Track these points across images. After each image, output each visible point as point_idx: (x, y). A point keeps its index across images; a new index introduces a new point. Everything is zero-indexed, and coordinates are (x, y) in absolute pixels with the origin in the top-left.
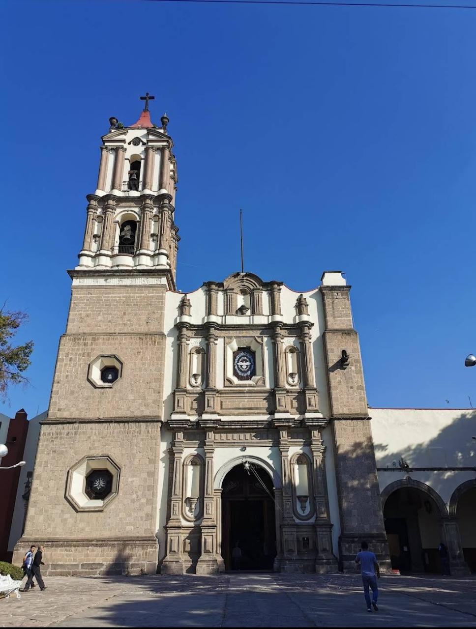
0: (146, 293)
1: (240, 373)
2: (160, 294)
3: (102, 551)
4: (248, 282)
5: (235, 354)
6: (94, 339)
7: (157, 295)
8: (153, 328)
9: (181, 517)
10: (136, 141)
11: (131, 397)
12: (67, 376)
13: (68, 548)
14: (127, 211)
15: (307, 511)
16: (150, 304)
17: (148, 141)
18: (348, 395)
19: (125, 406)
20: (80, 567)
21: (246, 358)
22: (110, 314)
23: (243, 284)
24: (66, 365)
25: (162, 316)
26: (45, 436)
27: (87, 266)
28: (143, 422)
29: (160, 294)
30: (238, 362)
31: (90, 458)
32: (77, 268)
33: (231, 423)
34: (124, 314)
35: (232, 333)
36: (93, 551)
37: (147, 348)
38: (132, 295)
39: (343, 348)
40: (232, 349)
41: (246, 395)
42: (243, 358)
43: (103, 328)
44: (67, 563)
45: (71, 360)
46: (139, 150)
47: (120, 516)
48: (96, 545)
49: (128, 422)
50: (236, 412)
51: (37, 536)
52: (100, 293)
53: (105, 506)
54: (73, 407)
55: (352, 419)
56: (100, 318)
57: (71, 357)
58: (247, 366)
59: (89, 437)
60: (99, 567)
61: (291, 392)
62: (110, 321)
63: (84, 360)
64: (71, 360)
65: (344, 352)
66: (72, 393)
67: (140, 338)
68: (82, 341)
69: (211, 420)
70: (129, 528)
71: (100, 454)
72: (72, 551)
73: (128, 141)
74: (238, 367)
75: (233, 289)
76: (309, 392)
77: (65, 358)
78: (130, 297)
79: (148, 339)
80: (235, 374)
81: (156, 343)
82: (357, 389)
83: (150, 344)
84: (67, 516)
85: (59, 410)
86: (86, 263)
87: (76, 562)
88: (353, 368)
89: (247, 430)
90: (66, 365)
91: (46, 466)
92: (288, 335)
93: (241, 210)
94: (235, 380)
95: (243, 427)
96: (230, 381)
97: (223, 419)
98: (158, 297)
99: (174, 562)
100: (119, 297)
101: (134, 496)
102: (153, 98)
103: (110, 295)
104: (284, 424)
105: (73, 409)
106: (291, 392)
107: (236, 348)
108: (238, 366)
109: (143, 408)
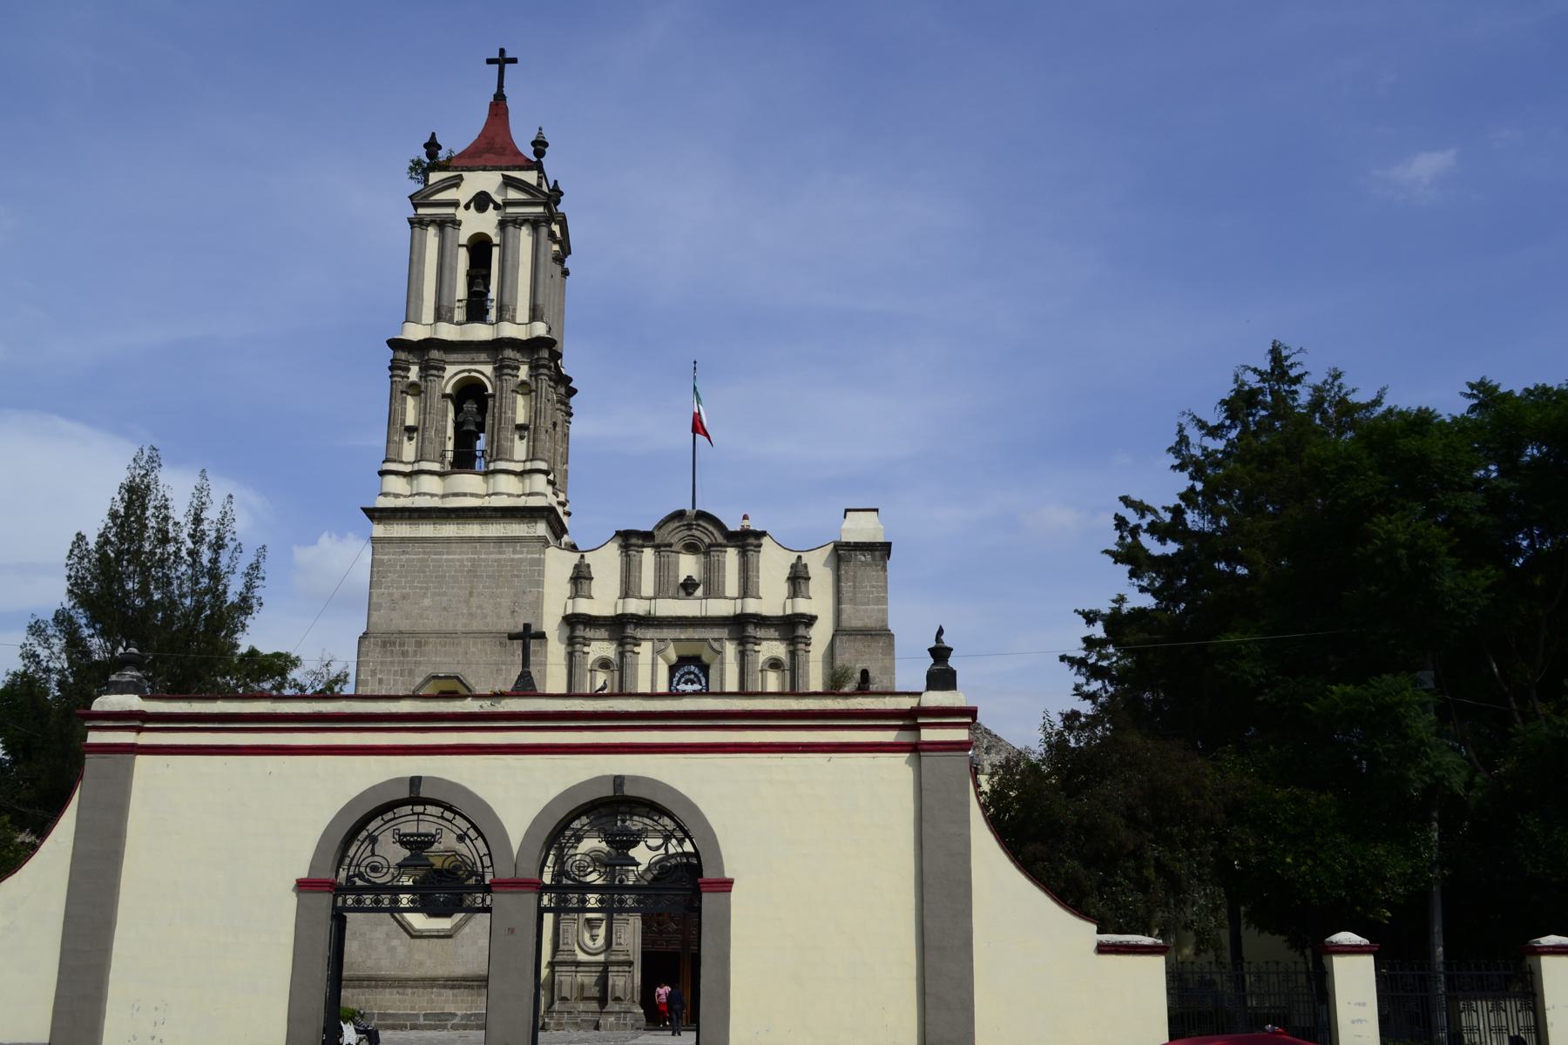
3: (453, 995)
5: (673, 669)
6: (419, 644)
7: (529, 556)
10: (481, 201)
13: (401, 990)
14: (469, 371)
16: (517, 576)
20: (421, 1018)
21: (692, 676)
22: (445, 594)
23: (690, 533)
30: (678, 684)
36: (440, 995)
38: (483, 556)
39: (864, 666)
40: (666, 659)
42: (687, 677)
44: (401, 1012)
46: (487, 222)
48: (445, 987)
51: (408, 973)
52: (424, 553)
53: (457, 928)
56: (427, 602)
67: (500, 643)
75: (670, 545)
77: (369, 678)
78: (480, 559)
84: (396, 942)
100: (458, 560)
107: (674, 658)
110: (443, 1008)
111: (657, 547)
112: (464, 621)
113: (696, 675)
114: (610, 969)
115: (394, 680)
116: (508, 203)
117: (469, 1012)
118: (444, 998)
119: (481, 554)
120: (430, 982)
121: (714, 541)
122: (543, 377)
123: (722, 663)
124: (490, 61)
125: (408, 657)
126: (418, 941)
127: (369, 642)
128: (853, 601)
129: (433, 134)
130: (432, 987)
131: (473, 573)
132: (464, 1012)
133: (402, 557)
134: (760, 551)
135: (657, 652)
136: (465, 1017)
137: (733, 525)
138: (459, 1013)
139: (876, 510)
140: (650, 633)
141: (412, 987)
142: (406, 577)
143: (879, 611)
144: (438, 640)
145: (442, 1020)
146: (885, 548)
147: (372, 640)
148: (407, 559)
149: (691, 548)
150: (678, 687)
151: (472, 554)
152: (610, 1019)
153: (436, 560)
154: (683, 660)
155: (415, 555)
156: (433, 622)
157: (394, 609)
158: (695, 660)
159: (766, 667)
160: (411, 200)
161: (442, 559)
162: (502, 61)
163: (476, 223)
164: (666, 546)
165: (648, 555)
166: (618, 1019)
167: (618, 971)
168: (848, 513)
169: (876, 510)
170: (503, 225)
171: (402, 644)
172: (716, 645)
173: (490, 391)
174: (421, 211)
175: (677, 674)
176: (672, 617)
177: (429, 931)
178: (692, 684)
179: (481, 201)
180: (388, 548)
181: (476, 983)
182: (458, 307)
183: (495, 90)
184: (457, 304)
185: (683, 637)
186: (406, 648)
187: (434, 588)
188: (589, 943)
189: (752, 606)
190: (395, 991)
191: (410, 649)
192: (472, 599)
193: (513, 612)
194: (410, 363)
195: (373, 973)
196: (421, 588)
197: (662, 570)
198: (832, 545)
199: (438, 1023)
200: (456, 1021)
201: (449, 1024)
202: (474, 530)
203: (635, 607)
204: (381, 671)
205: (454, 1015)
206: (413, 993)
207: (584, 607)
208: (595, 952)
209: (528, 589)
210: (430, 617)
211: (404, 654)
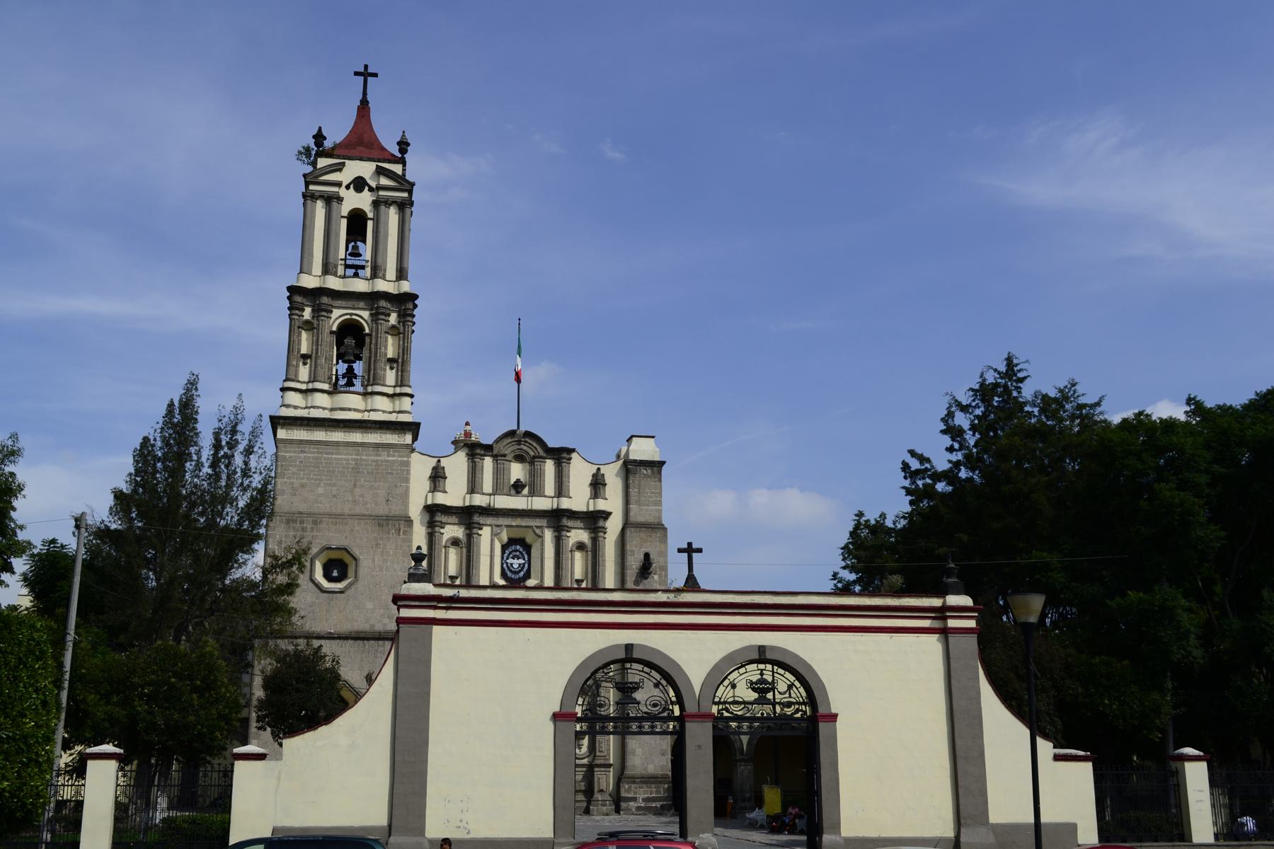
1: (509, 574)
5: (504, 548)
6: (315, 523)
7: (400, 459)
11: (369, 605)
14: (351, 314)
16: (390, 474)
21: (518, 553)
23: (519, 447)
30: (507, 559)
38: (364, 458)
39: (647, 550)
40: (500, 540)
42: (514, 553)
49: (368, 639)
52: (318, 452)
56: (320, 490)
58: (520, 565)
65: (647, 556)
75: (505, 456)
78: (361, 460)
83: (393, 534)
88: (656, 577)
92: (366, 307)
108: (507, 563)
112: (350, 506)
116: (379, 188)
123: (542, 544)
124: (356, 74)
125: (306, 532)
128: (638, 503)
129: (320, 128)
131: (357, 470)
133: (301, 455)
135: (494, 535)
140: (490, 520)
142: (304, 470)
147: (278, 517)
149: (520, 458)
150: (507, 561)
154: (512, 541)
155: (311, 454)
156: (324, 506)
157: (295, 495)
160: (307, 184)
162: (366, 74)
165: (488, 462)
172: (538, 531)
175: (507, 551)
179: (359, 184)
183: (361, 97)
191: (308, 526)
192: (355, 490)
193: (388, 501)
197: (499, 474)
202: (357, 437)
203: (479, 500)
207: (441, 499)
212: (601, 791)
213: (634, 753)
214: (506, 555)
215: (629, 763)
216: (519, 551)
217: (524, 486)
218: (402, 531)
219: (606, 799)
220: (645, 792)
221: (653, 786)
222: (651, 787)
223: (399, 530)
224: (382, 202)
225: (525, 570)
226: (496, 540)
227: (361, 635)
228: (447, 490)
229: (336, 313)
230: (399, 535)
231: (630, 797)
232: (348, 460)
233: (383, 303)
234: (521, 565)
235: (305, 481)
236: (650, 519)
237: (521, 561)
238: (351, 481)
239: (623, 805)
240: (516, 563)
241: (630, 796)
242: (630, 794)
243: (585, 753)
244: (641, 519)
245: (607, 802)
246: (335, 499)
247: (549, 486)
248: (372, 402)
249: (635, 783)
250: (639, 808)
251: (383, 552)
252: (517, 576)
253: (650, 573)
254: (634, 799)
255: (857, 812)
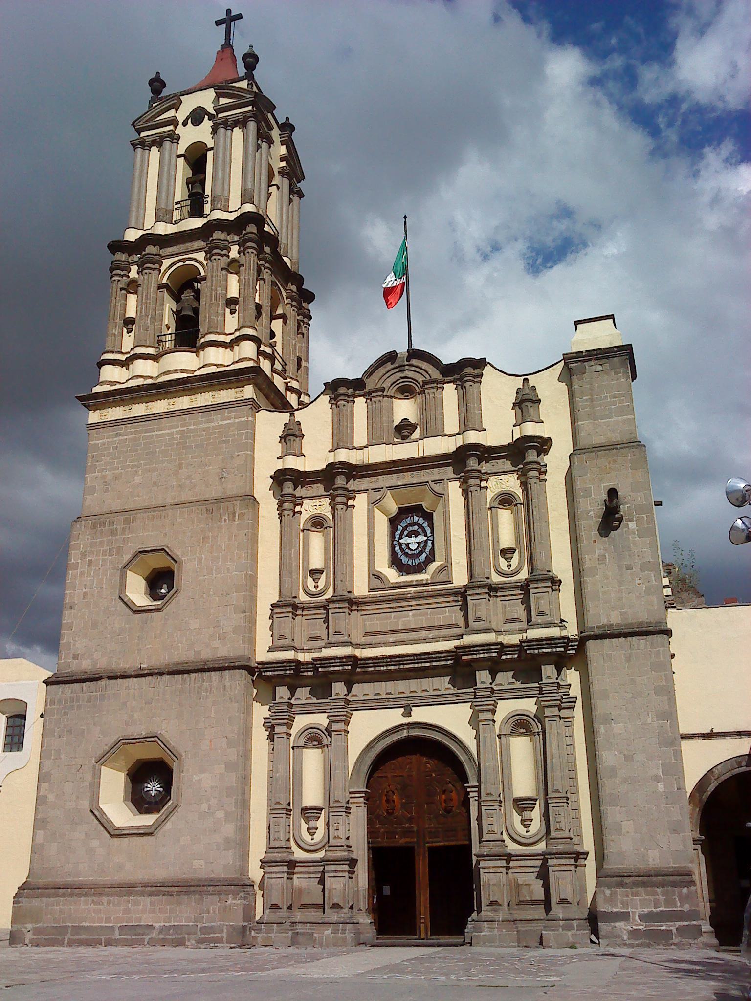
0: (217, 420)
1: (404, 559)
2: (243, 419)
3: (152, 903)
4: (413, 368)
5: (393, 522)
6: (127, 521)
7: (237, 421)
8: (233, 487)
9: (505, 836)
10: (198, 115)
11: (194, 624)
12: (85, 594)
13: (95, 899)
14: (184, 260)
15: (320, 835)
16: (225, 442)
17: (219, 110)
18: (620, 583)
19: (184, 642)
20: (117, 932)
21: (416, 528)
22: (155, 469)
23: (403, 375)
24: (82, 573)
25: (251, 460)
26: (54, 705)
27: (112, 383)
28: (214, 669)
29: (243, 419)
30: (401, 538)
31: (126, 741)
32: (97, 389)
33: (376, 661)
34: (180, 466)
35: (384, 481)
36: (136, 903)
37: (220, 528)
38: (192, 427)
39: (611, 485)
40: (384, 512)
41: (410, 603)
42: (410, 529)
43: (142, 500)
44: (96, 925)
45: (90, 563)
46: (203, 133)
47: (182, 843)
48: (142, 894)
49: (188, 672)
50: (391, 638)
51: (50, 880)
52: (136, 432)
53: (158, 825)
54: (96, 650)
55: (626, 635)
56: (138, 480)
57: (90, 558)
58: (419, 543)
59: (125, 704)
60: (147, 931)
61: (503, 588)
62: (155, 483)
63: (112, 562)
64: (90, 563)
65: (613, 493)
66: (95, 625)
67: (207, 510)
68: (107, 528)
69: (335, 658)
70: (196, 864)
71: (144, 734)
72: (103, 904)
73: (181, 120)
74: (401, 548)
75: (383, 390)
76: (536, 585)
77: (79, 561)
78: (189, 431)
79: (222, 510)
80: (395, 562)
81: (237, 517)
82: (642, 570)
83: (225, 520)
84: (95, 843)
85: (75, 657)
86: (112, 375)
87: (110, 923)
88: (632, 525)
89: (411, 674)
90: (82, 573)
91: (58, 758)
92: (455, 476)
93: (405, 217)
94: (392, 576)
95: (402, 667)
96: (378, 576)
97: (361, 653)
98: (240, 426)
99: (275, 925)
100: (169, 435)
101: (204, 807)
102: (239, 17)
103: (154, 433)
104: (481, 656)
105: (97, 655)
106: (503, 588)
107: (394, 508)
108: (400, 544)
109: (216, 643)
110: (140, 919)
111: (368, 395)
112: (173, 493)
113: (420, 526)
114: (550, 862)
115: (103, 560)
116: (219, 110)
117: (167, 924)
118: (141, 907)
119: (190, 426)
120: (127, 888)
121: (428, 378)
122: (250, 250)
123: (446, 506)
125: (117, 535)
126: (117, 841)
127: (80, 526)
128: (592, 416)
130: (129, 894)
132: (162, 924)
133: (115, 439)
134: (480, 382)
136: (162, 930)
137: (449, 355)
138: (157, 925)
139: (611, 317)
140: (365, 483)
141: (108, 895)
142: (118, 458)
143: (624, 422)
144: (146, 515)
145: (139, 934)
146: (626, 352)
147: (83, 522)
148: (119, 440)
149: (406, 391)
150: (401, 541)
151: (181, 427)
152: (326, 932)
153: (148, 437)
154: (404, 512)
155: (128, 433)
157: (107, 490)
158: (417, 509)
159: (496, 504)
160: (134, 126)
161: (153, 435)
163: (189, 135)
164: (377, 391)
165: (360, 404)
166: (335, 932)
167: (336, 872)
168: (578, 326)
169: (611, 317)
170: (215, 131)
171: (112, 523)
172: (437, 488)
173: (203, 274)
174: (143, 134)
175: (399, 527)
176: (386, 463)
177: (128, 828)
178: (416, 537)
179: (198, 115)
180: (102, 433)
181: (176, 889)
182: (176, 209)
184: (175, 206)
185: (400, 484)
186: (115, 527)
187: (145, 464)
188: (307, 837)
189: (473, 437)
190: (90, 899)
191: (119, 527)
192: (180, 471)
194: (130, 264)
195: (70, 879)
196: (132, 467)
198: (563, 363)
199: (133, 937)
200: (154, 935)
201: (147, 938)
204: (91, 553)
205: (151, 927)
206: (109, 903)
207: (292, 463)
208: (312, 848)
209: (236, 454)
210: (141, 495)
211: (113, 533)
212: (563, 901)
213: (619, 832)
214: (399, 532)
215: (611, 849)
216: (418, 525)
217: (413, 427)
218: (237, 515)
219: (572, 916)
220: (643, 903)
221: (659, 890)
222: (656, 894)
223: (234, 514)
224: (220, 124)
225: (427, 550)
226: (376, 510)
227: (180, 668)
228: (303, 452)
229: (166, 263)
230: (234, 521)
231: (616, 913)
232: (172, 433)
233: (218, 235)
234: (422, 546)
235: (120, 471)
236: (615, 437)
237: (421, 538)
238: (175, 461)
239: (603, 926)
240: (413, 542)
241: (615, 910)
242: (617, 906)
243: (539, 831)
244: (597, 440)
245: (575, 923)
246: (155, 488)
247: (451, 423)
248: (204, 354)
249: (621, 885)
250: (634, 933)
251: (212, 546)
252: (417, 561)
253: (620, 520)
254: (624, 916)
255: (212, 863)
